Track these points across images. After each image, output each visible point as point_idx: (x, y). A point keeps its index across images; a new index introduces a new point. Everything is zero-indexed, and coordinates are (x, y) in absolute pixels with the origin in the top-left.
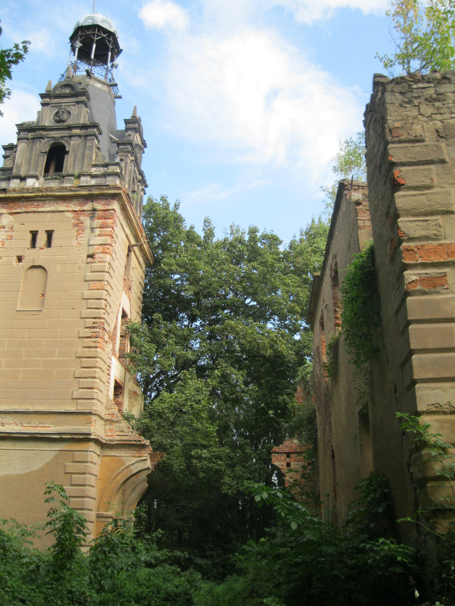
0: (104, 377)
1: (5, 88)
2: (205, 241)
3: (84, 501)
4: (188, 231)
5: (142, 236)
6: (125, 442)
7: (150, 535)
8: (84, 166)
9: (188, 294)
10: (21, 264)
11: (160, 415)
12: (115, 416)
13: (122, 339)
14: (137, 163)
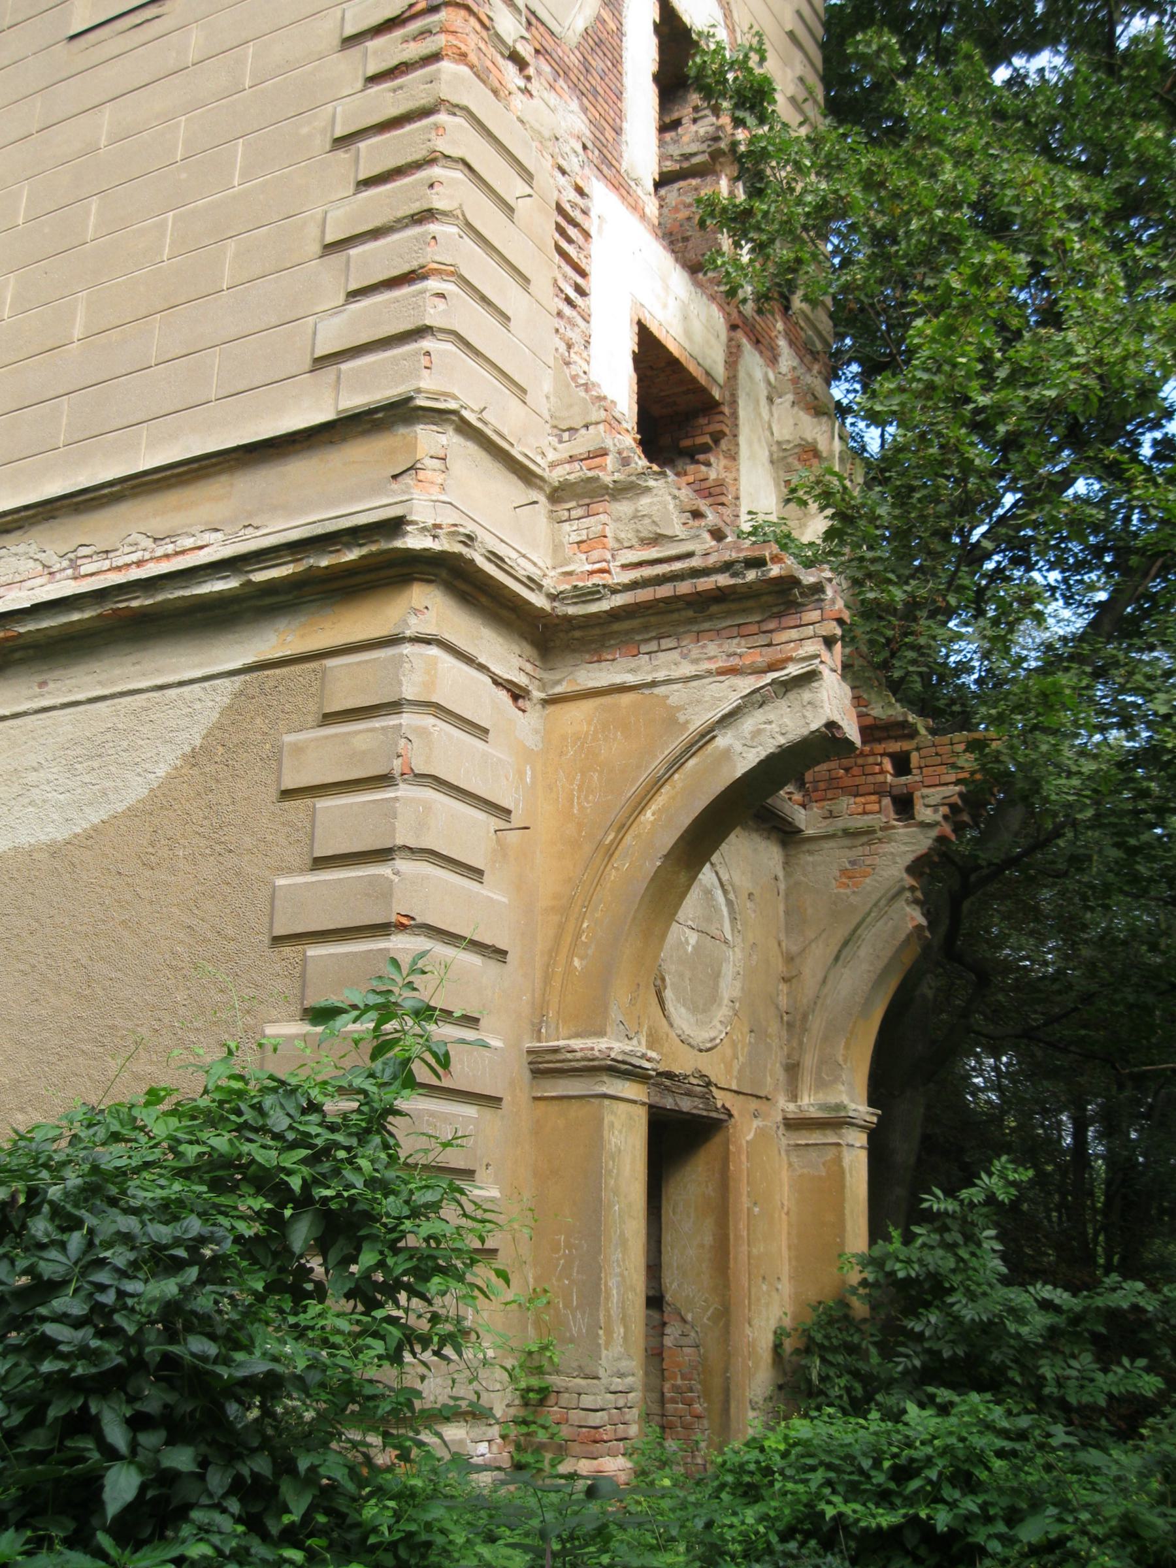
6: (665, 591)
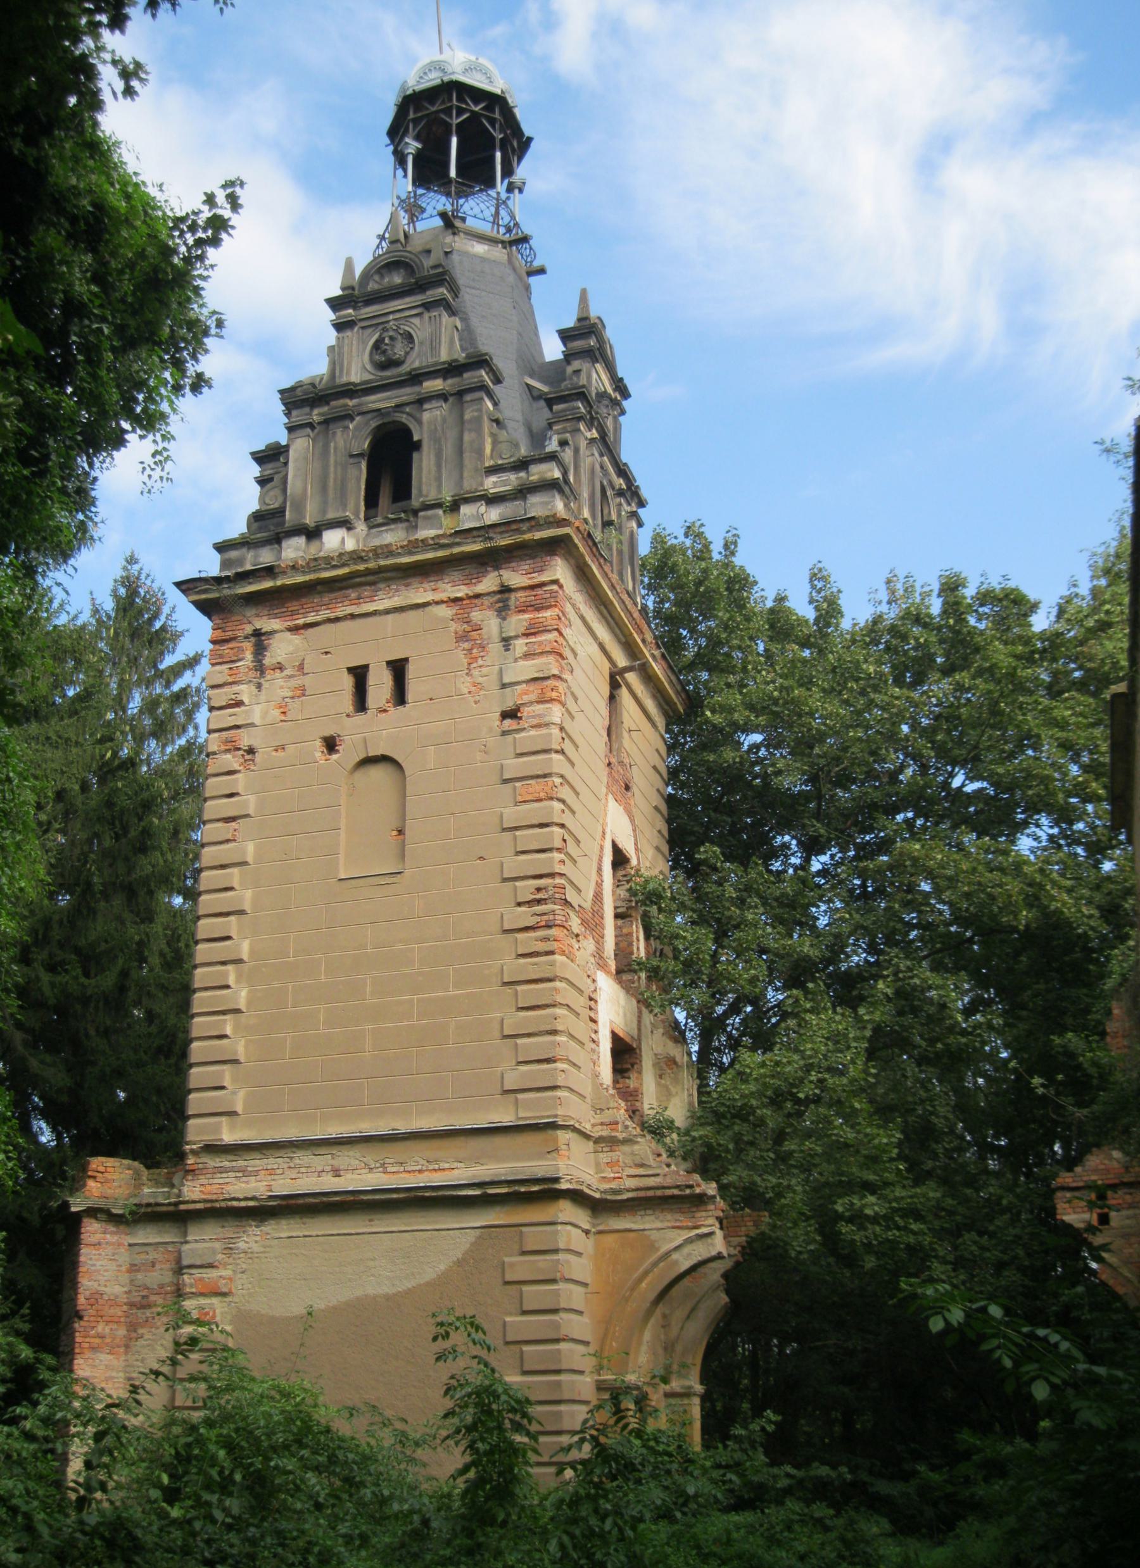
0: (580, 1028)
1: (205, 311)
2: (820, 630)
3: (559, 1351)
4: (772, 611)
5: (644, 641)
6: (650, 1193)
7: (746, 1428)
8: (465, 474)
9: (794, 782)
10: (335, 757)
11: (742, 1114)
12: (620, 1127)
13: (620, 922)
14: (607, 445)
